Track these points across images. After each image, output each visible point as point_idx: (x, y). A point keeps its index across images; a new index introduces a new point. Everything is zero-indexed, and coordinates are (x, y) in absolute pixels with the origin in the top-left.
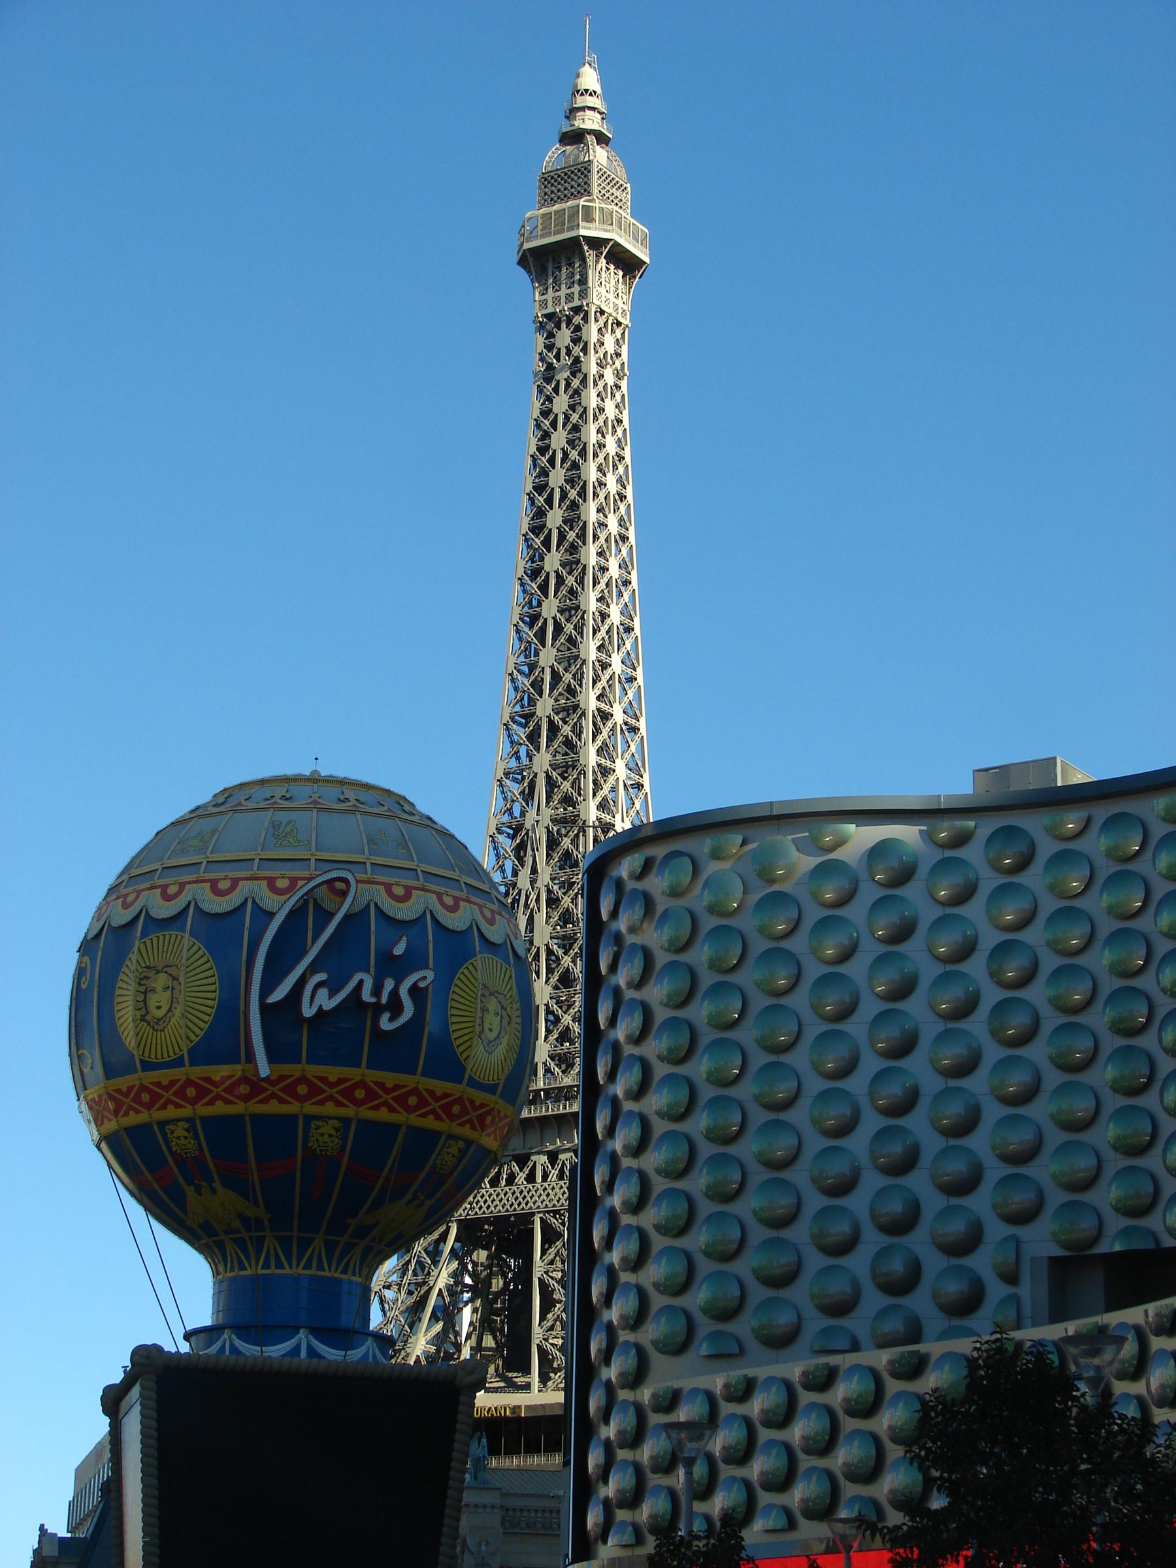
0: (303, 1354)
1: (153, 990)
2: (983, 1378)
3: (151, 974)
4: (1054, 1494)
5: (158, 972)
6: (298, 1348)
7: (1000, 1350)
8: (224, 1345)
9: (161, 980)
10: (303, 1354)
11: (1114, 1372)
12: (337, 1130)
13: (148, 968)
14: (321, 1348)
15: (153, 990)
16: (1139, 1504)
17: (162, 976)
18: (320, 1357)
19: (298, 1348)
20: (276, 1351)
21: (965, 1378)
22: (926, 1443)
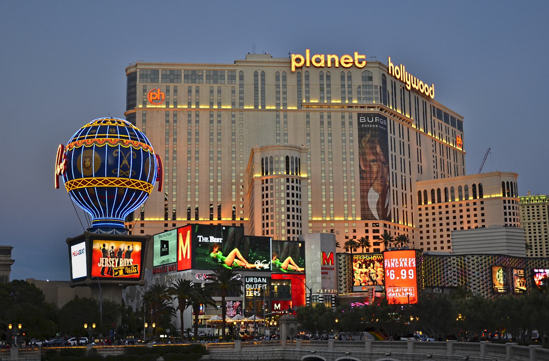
0: (114, 233)
1: (86, 161)
2: (415, 319)
3: (86, 158)
4: (279, 305)
5: (87, 158)
6: (113, 232)
7: (299, 305)
8: (98, 231)
9: (88, 159)
10: (114, 233)
11: (493, 171)
12: (124, 190)
13: (85, 157)
14: (118, 232)
15: (86, 161)
16: (262, 241)
17: (88, 159)
18: (101, 233)
19: (113, 232)
20: (95, 232)
21: (233, 232)
22: (23, 343)
